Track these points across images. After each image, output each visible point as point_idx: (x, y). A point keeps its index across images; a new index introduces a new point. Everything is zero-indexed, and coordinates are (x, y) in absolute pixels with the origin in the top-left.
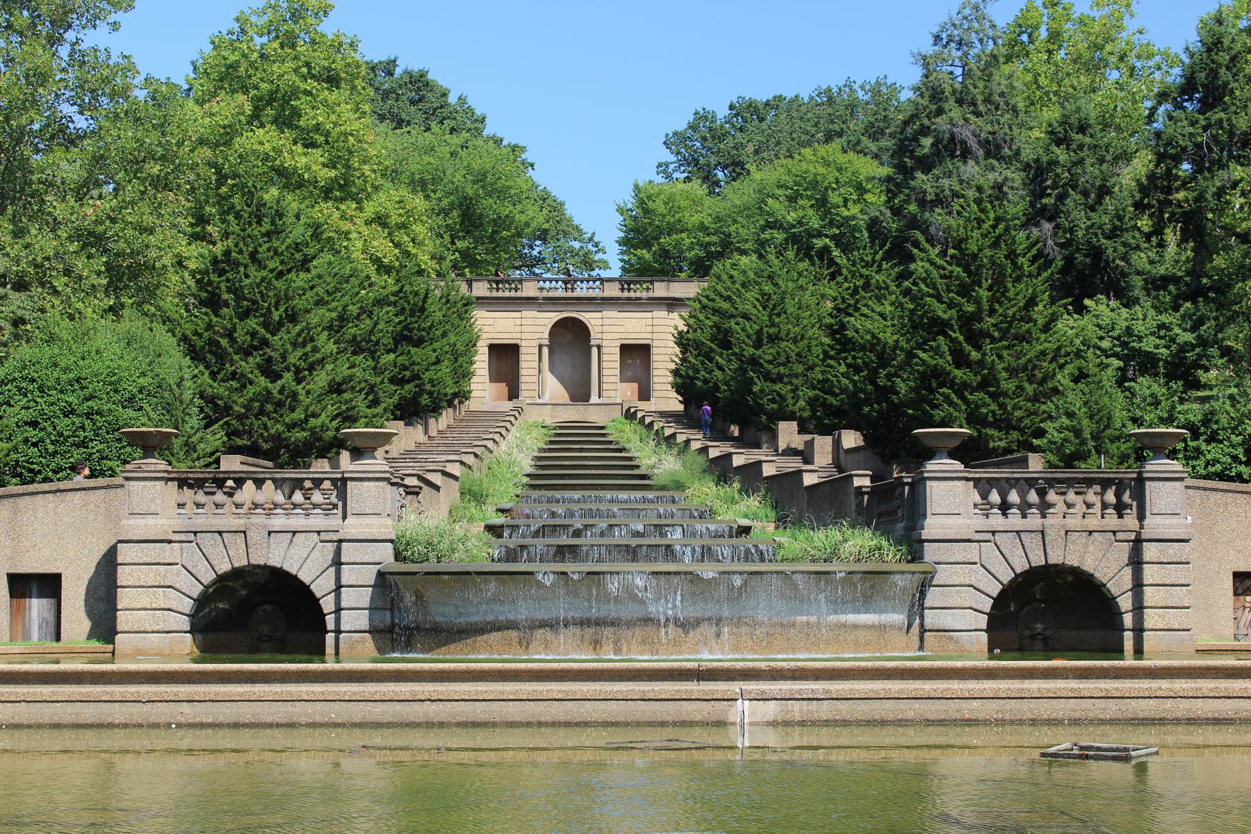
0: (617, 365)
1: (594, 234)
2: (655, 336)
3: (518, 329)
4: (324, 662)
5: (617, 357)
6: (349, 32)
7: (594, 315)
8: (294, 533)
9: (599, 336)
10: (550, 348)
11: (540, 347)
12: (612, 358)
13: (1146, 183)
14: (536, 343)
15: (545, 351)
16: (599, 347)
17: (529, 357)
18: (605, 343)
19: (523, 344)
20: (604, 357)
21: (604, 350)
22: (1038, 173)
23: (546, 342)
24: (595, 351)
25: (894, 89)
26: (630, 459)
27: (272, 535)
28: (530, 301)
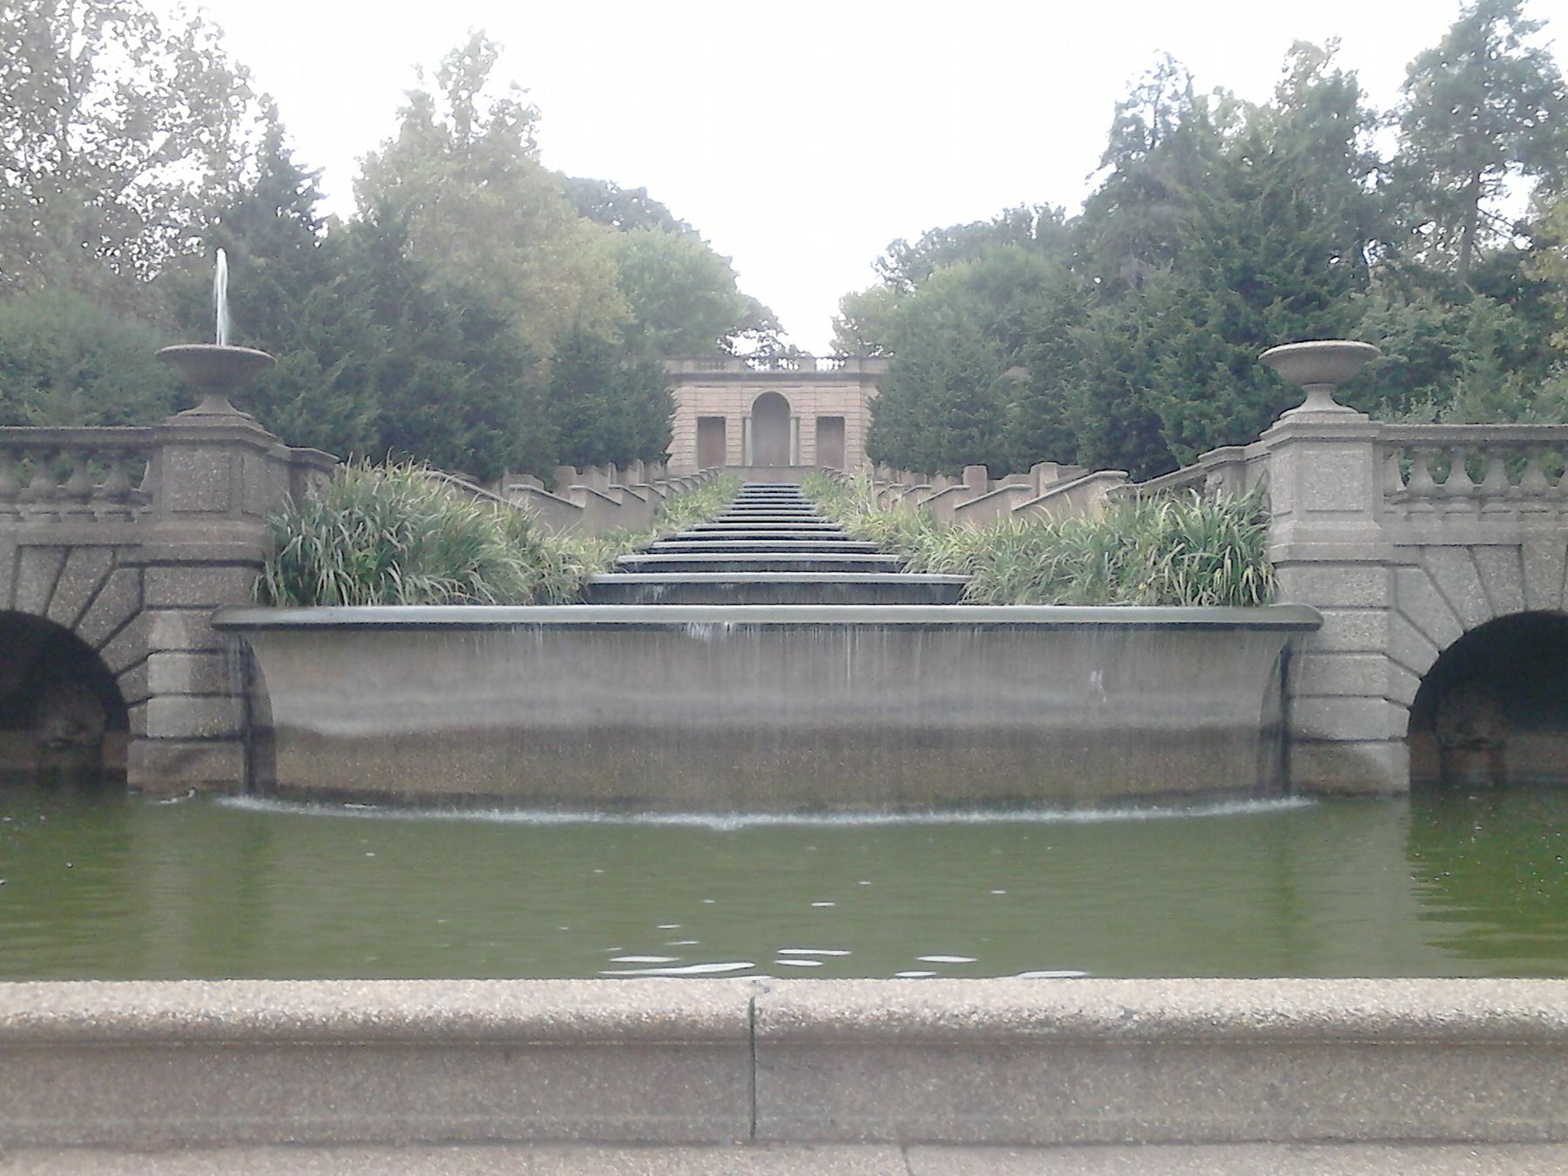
0: (813, 436)
2: (848, 409)
3: (699, 396)
5: (813, 429)
8: (68, 549)
9: (798, 409)
11: (744, 420)
12: (809, 429)
15: (748, 422)
16: (798, 419)
19: (729, 417)
21: (801, 422)
23: (750, 415)
24: (793, 423)
27: (26, 552)
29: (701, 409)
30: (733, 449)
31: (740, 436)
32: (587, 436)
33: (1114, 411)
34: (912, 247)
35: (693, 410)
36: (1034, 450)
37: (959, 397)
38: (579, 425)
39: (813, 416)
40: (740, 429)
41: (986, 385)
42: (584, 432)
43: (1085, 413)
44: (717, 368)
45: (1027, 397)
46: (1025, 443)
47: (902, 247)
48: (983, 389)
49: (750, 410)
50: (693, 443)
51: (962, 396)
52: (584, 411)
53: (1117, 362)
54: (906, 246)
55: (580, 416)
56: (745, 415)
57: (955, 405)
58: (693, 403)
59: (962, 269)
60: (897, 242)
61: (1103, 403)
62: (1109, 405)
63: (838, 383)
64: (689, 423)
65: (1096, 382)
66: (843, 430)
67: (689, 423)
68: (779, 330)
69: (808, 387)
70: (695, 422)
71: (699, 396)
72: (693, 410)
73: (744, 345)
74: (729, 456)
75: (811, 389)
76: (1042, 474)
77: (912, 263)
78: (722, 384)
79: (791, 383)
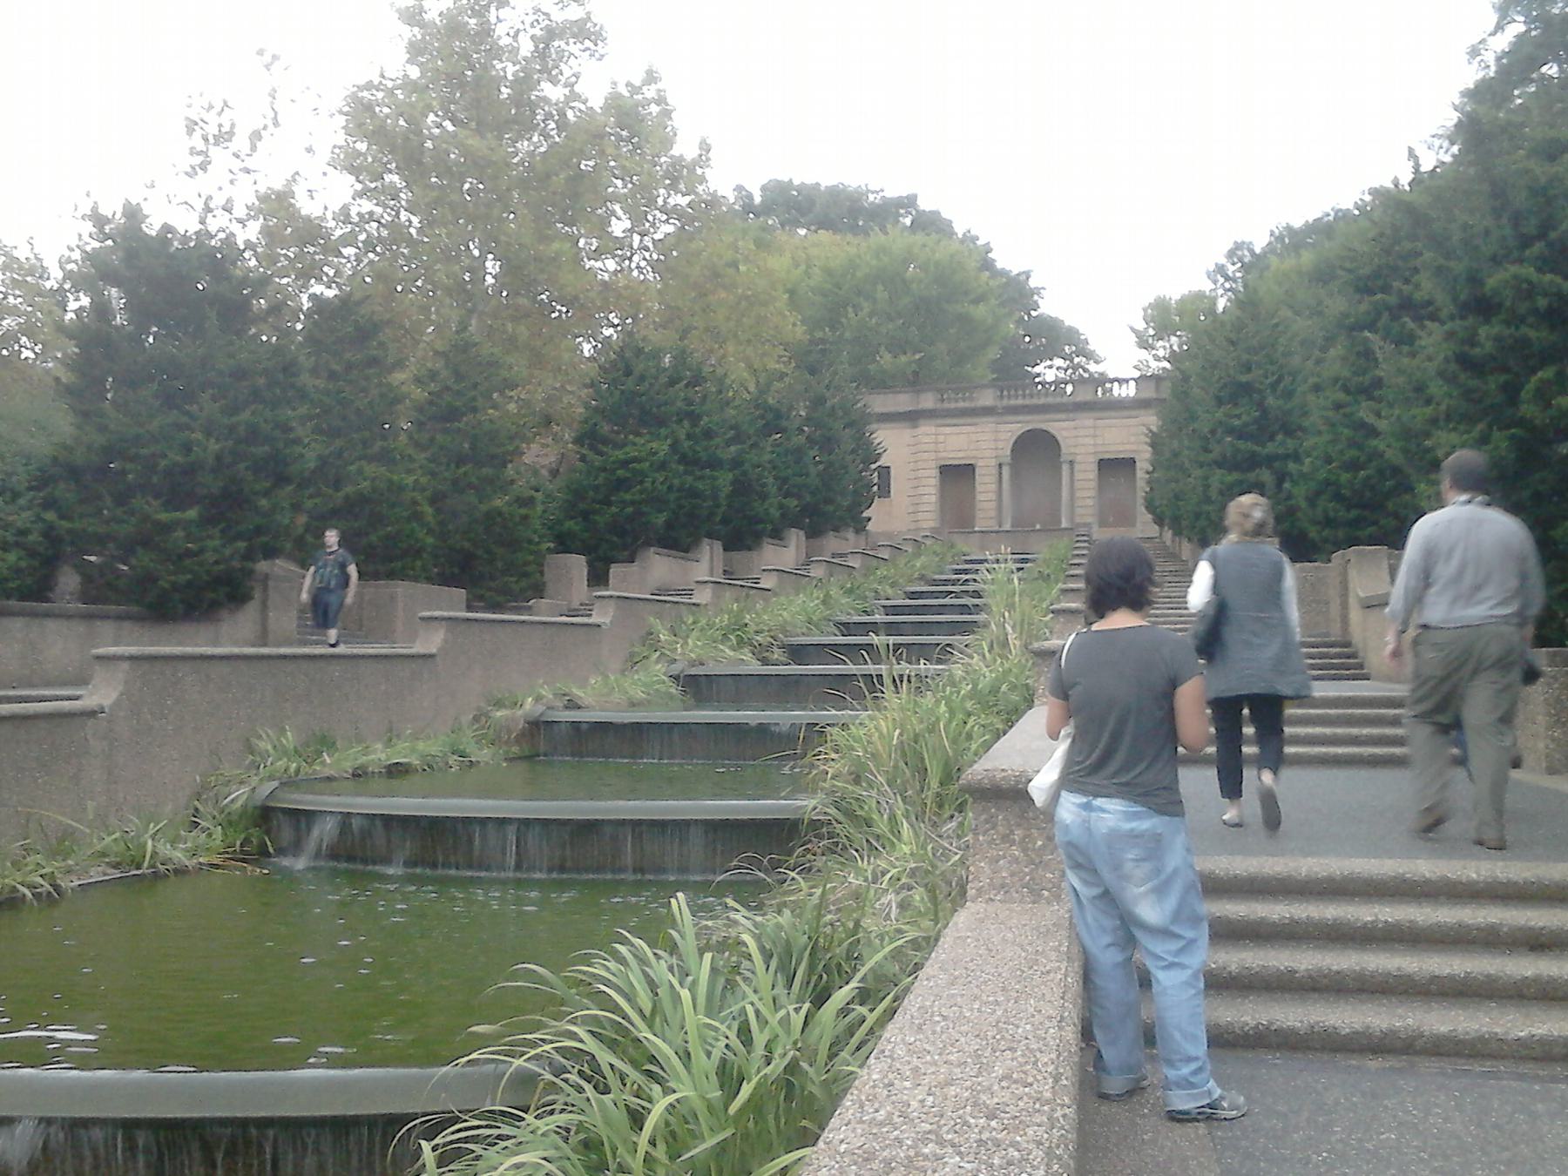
0: (1093, 484)
1: (1132, 329)
3: (941, 438)
4: (607, 590)
6: (606, 90)
7: (1065, 424)
9: (1072, 450)
10: (1012, 466)
12: (1087, 475)
13: (758, 200)
14: (993, 462)
17: (987, 479)
18: (1079, 458)
19: (980, 463)
20: (1078, 476)
21: (1077, 467)
22: (651, 202)
23: (1008, 460)
24: (1065, 468)
25: (668, 142)
26: (1361, 666)
28: (988, 411)
29: (944, 455)
30: (986, 505)
31: (994, 487)
32: (633, 503)
33: (1528, 409)
34: (1258, 250)
35: (933, 455)
36: (1354, 513)
37: (1239, 417)
38: (621, 485)
39: (933, 464)
40: (994, 479)
41: (1289, 394)
42: (628, 497)
43: (1434, 421)
44: (964, 401)
45: (1338, 406)
46: (1338, 497)
47: (1246, 253)
48: (1280, 402)
49: (1009, 453)
50: (933, 499)
51: (1245, 414)
52: (625, 464)
53: (1538, 248)
54: (1252, 252)
55: (620, 472)
56: (1001, 460)
57: (1231, 431)
58: (932, 447)
59: (1307, 258)
60: (1238, 246)
61: (1493, 383)
62: (1511, 393)
63: (1126, 413)
64: (926, 473)
65: (1470, 321)
66: (974, 478)
67: (926, 473)
68: (1090, 356)
69: (1086, 420)
70: (936, 472)
71: (941, 438)
72: (933, 455)
73: (1048, 371)
74: (979, 514)
75: (1089, 422)
76: (1353, 574)
77: (1252, 264)
78: (969, 420)
79: (1063, 416)
